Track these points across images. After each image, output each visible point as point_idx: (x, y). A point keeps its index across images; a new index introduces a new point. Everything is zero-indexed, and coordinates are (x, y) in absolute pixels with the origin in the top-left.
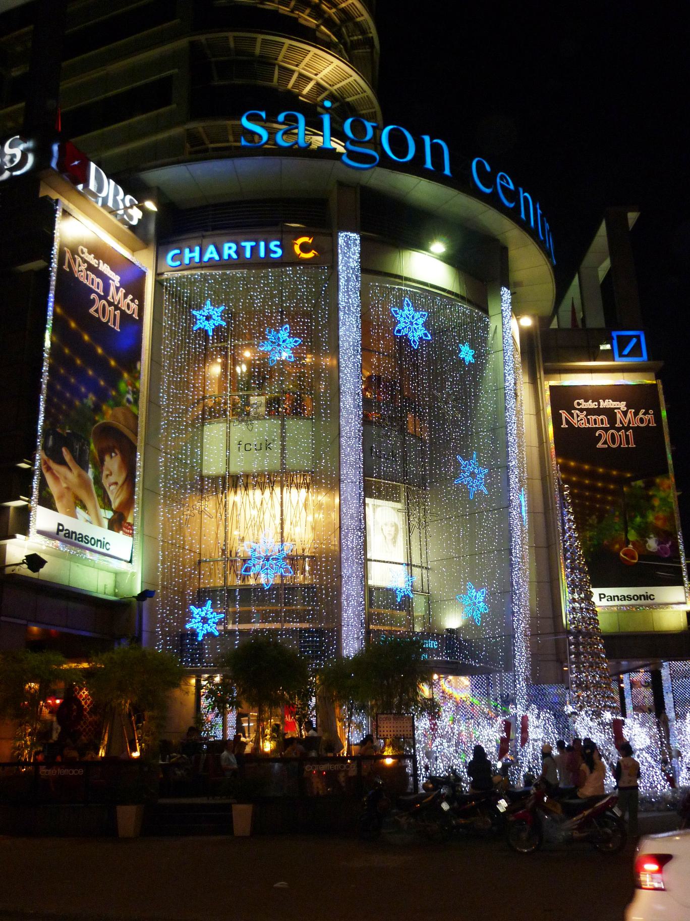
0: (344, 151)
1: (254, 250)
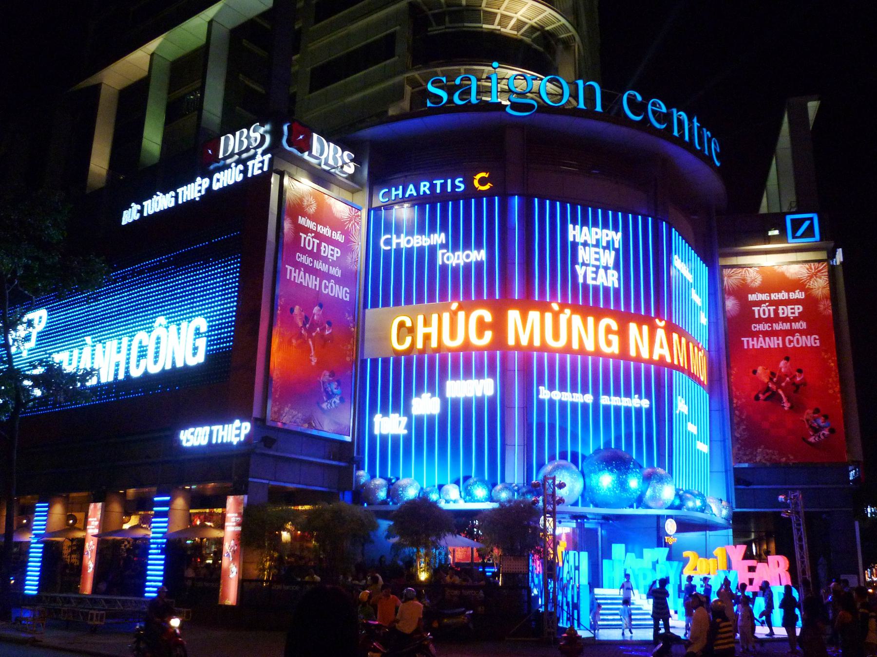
0: (508, 103)
1: (444, 186)
